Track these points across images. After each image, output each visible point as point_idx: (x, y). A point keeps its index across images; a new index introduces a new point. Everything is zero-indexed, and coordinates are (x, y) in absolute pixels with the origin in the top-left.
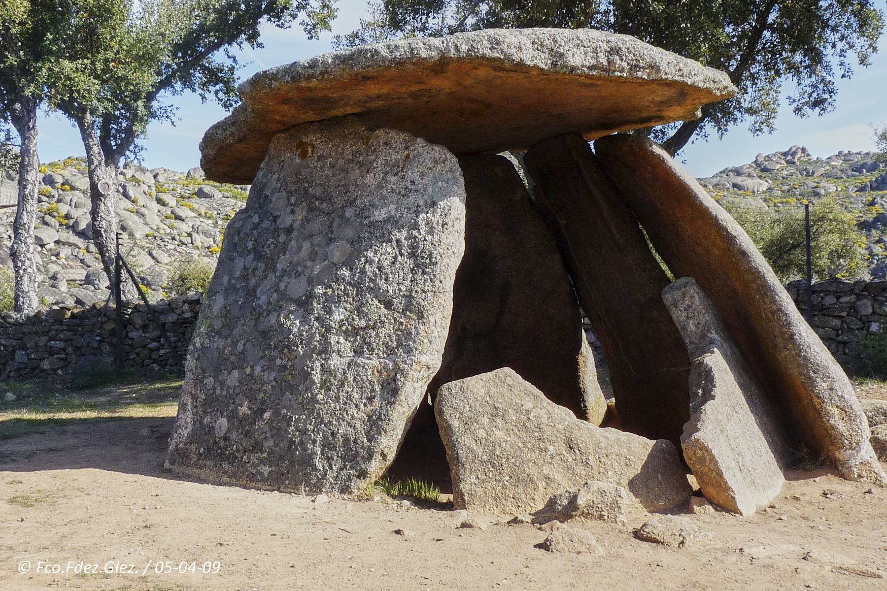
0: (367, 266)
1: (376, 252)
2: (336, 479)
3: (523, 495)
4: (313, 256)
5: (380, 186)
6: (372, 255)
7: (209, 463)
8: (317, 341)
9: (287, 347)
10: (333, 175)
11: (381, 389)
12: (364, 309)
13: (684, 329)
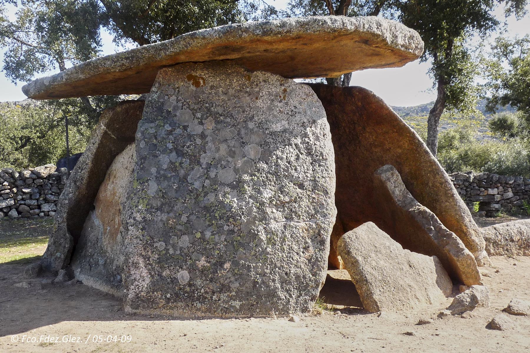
0: (279, 161)
1: (283, 152)
2: (296, 303)
3: (403, 298)
4: (232, 154)
5: (270, 109)
6: (280, 154)
7: (180, 304)
8: (255, 212)
9: (230, 216)
10: (229, 100)
11: (312, 241)
12: (286, 190)
13: (393, 193)
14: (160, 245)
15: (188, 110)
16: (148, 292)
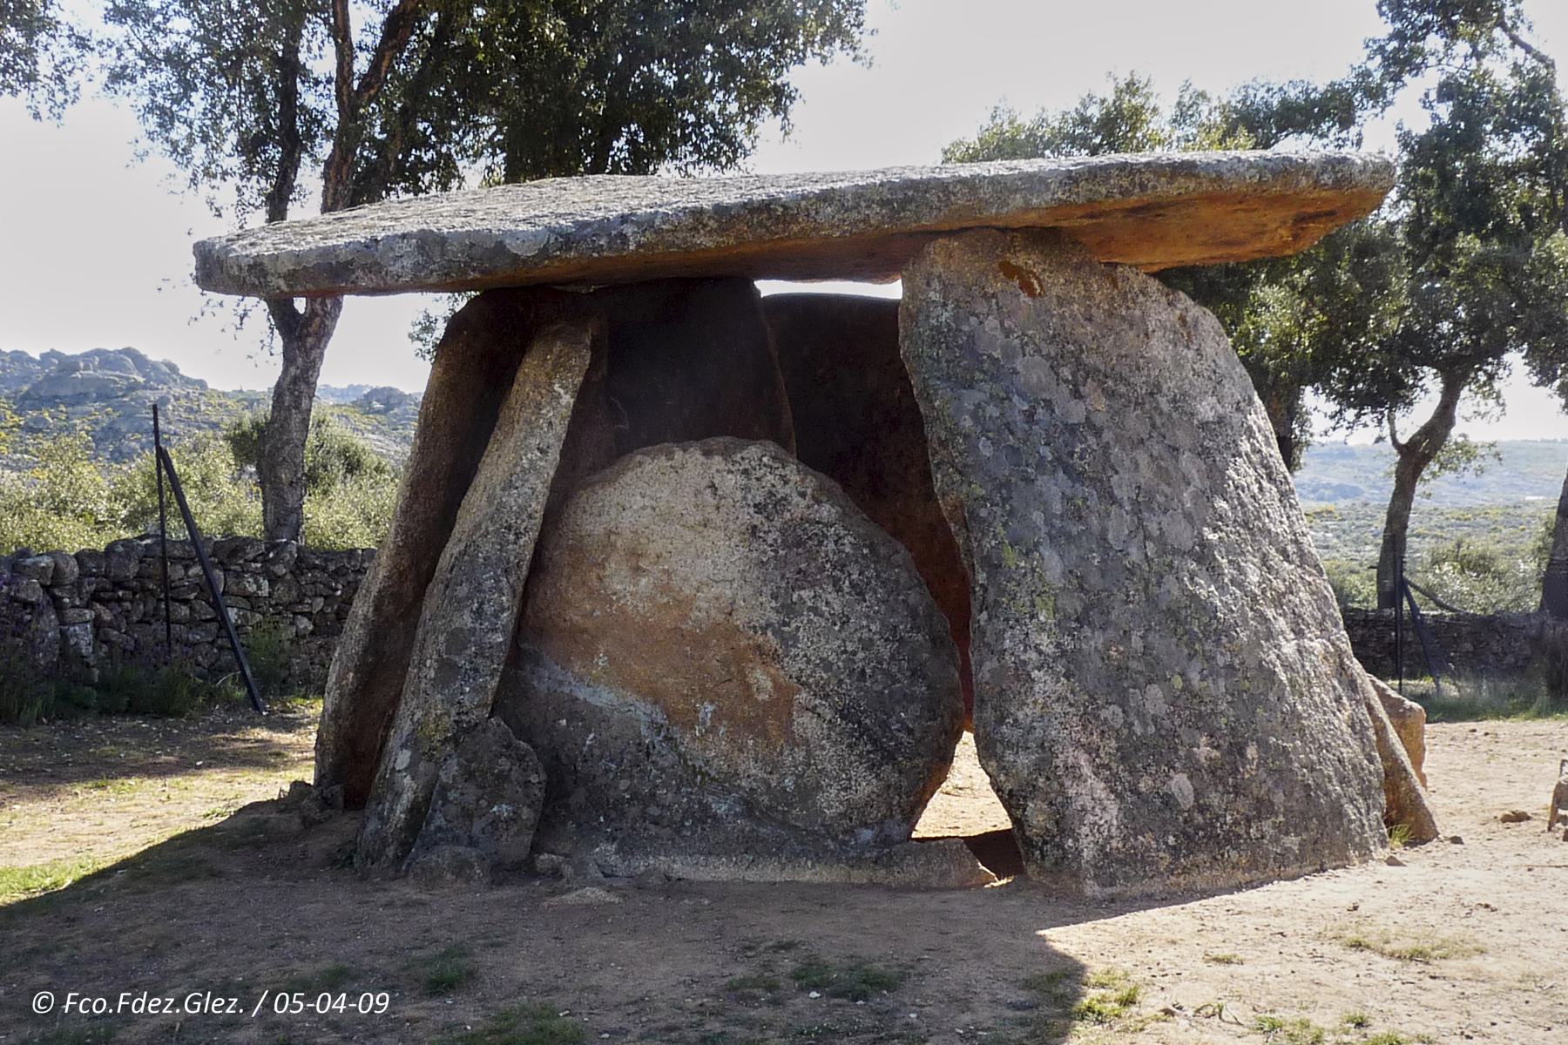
9: (1220, 633)
14: (1112, 713)
15: (1037, 358)
16: (1125, 839)
